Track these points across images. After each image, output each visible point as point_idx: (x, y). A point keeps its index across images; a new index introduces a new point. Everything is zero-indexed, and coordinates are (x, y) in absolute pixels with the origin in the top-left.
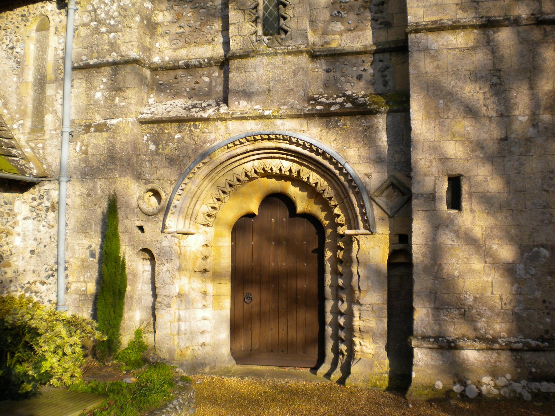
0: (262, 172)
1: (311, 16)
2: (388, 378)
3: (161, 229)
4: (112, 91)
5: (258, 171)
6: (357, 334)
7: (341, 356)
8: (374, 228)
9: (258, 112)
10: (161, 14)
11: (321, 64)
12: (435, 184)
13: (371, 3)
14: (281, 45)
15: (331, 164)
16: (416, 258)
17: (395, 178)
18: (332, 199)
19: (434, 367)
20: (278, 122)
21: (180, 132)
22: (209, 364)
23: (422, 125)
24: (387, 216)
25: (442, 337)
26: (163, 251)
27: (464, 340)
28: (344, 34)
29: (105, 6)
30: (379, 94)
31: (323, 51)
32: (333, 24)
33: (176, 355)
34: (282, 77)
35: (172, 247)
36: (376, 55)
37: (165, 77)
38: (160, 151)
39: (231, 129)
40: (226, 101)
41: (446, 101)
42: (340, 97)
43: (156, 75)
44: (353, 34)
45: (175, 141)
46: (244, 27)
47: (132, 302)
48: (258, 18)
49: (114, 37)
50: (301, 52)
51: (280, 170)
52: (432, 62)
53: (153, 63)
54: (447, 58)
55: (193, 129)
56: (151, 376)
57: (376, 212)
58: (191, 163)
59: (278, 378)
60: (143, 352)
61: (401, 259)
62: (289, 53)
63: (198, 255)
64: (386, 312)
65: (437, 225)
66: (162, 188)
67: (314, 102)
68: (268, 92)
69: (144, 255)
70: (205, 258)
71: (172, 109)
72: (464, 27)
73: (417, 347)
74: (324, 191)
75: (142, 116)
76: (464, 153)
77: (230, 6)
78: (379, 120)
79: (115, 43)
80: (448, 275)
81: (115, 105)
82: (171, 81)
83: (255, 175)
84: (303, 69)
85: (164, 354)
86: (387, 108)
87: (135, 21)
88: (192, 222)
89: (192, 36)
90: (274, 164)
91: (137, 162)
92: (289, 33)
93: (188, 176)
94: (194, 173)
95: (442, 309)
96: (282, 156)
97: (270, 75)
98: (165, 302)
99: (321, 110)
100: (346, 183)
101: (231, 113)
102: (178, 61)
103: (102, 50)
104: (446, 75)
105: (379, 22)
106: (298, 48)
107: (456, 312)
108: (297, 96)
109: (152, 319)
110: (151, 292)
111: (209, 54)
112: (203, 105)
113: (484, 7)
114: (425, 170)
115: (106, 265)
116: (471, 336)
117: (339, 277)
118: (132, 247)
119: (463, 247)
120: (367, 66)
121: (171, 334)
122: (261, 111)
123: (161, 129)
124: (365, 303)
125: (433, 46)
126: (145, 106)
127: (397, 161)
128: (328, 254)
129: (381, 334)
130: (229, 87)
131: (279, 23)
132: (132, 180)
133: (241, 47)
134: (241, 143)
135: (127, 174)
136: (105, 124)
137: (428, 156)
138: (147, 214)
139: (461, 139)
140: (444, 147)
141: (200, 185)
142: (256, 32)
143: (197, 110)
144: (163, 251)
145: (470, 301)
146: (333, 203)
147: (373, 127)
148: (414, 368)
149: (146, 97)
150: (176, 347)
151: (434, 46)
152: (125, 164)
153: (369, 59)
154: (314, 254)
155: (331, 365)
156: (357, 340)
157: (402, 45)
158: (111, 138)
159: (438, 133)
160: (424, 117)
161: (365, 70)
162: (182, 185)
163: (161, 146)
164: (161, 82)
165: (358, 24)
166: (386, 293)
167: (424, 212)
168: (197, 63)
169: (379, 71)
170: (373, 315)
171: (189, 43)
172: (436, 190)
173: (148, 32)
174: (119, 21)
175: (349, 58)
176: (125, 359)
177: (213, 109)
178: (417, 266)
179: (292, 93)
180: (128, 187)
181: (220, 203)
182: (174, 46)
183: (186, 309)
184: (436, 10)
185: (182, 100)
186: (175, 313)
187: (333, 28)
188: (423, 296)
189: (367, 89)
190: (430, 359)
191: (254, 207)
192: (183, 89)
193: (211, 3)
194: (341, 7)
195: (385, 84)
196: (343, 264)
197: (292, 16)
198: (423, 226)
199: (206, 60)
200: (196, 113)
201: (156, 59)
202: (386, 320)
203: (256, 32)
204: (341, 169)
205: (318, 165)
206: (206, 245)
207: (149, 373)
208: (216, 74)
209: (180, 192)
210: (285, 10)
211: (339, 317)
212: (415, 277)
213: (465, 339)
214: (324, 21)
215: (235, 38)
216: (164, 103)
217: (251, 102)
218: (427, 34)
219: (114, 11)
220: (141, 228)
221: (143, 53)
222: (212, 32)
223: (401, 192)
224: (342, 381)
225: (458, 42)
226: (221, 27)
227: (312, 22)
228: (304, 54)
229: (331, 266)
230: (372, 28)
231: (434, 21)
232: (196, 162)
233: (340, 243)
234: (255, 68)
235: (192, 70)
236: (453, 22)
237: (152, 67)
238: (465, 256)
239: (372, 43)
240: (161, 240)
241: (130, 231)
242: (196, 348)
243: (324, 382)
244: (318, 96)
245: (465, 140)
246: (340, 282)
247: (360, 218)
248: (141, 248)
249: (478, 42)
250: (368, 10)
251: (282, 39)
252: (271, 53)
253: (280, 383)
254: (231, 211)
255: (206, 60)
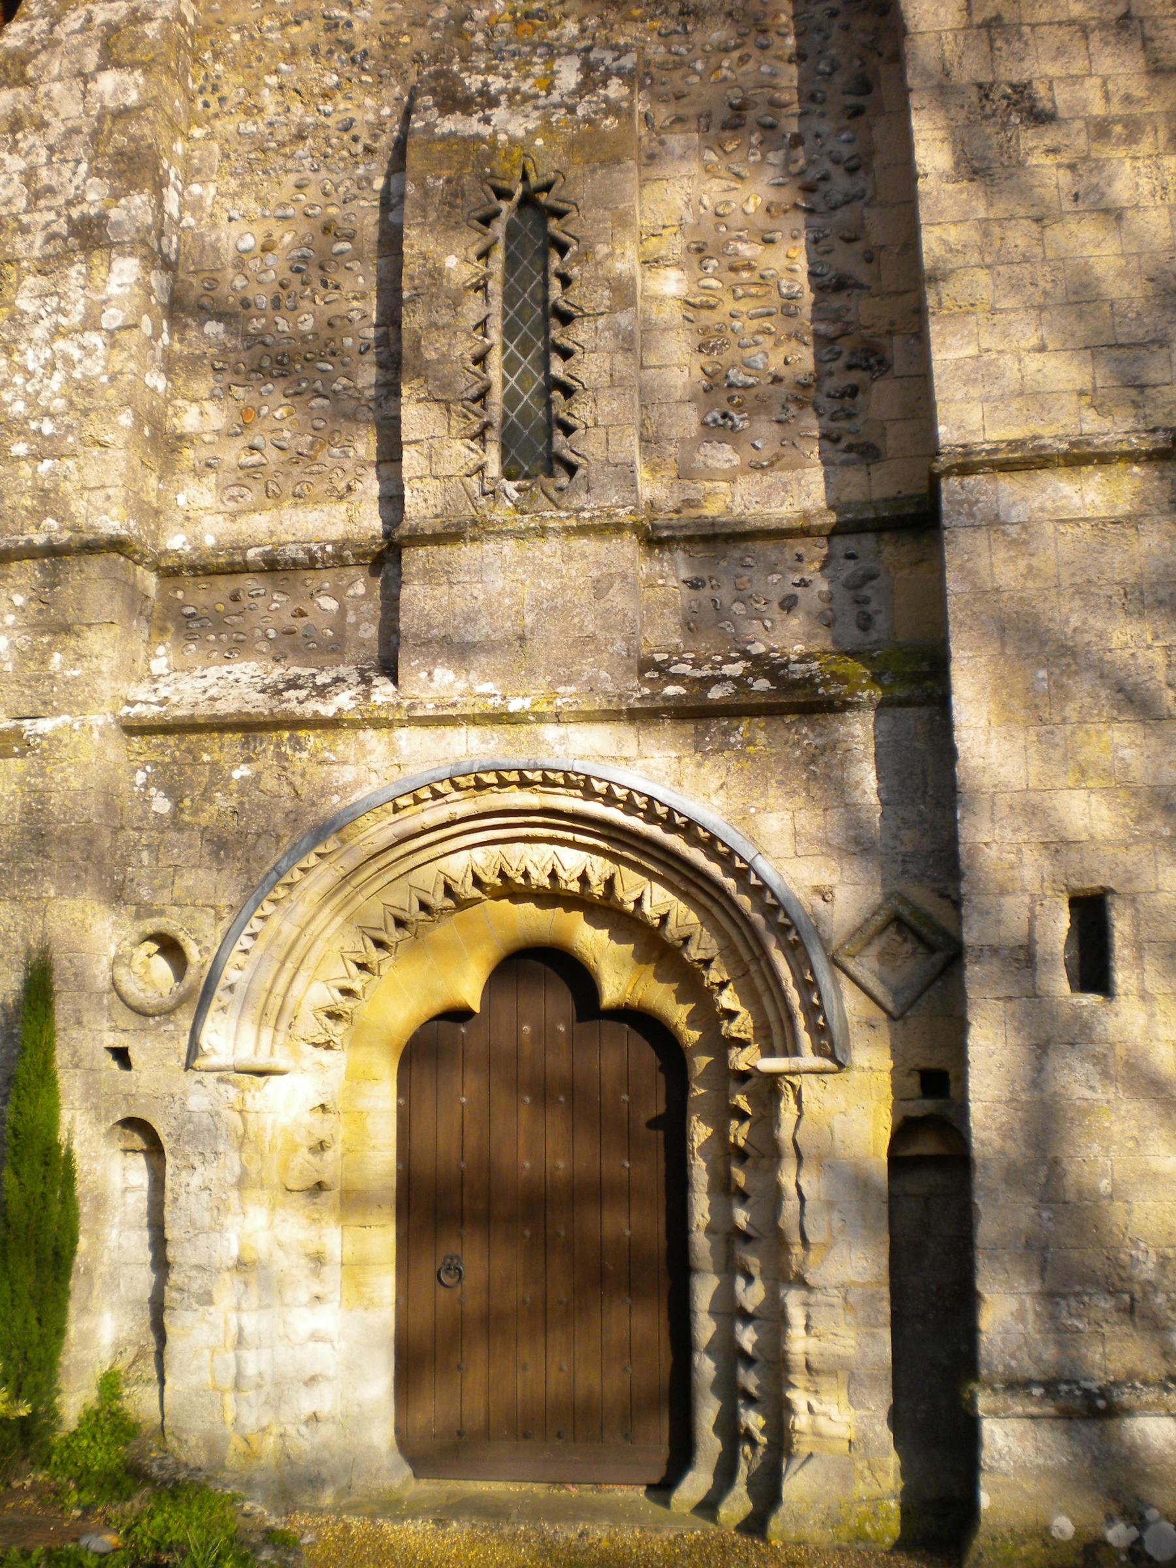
0: (498, 882)
1: (643, 425)
2: (898, 1513)
3: (184, 1058)
4: (43, 634)
5: (485, 879)
6: (798, 1378)
7: (747, 1448)
8: (847, 1051)
9: (491, 701)
10: (194, 409)
11: (674, 564)
12: (1032, 918)
13: (818, 389)
14: (558, 508)
15: (710, 858)
16: (982, 1143)
17: (904, 900)
18: (713, 965)
19: (1044, 1472)
20: (550, 732)
21: (248, 760)
22: (334, 1479)
23: (988, 742)
24: (884, 1015)
25: (1067, 1382)
26: (190, 1127)
27: (1134, 1387)
28: (740, 479)
29: (27, 380)
30: (847, 653)
31: (682, 527)
32: (707, 449)
33: (230, 1453)
34: (560, 601)
35: (218, 1114)
36: (836, 540)
37: (201, 595)
38: (186, 817)
39: (405, 752)
40: (390, 669)
41: (1057, 671)
42: (734, 661)
43: (176, 589)
44: (768, 479)
45: (233, 787)
46: (446, 452)
47: (91, 1286)
48: (487, 426)
49: (53, 473)
50: (619, 528)
51: (553, 876)
52: (1013, 559)
53: (165, 553)
54: (1057, 549)
55: (289, 752)
56: (168, 1529)
57: (849, 1005)
58: (279, 855)
59: (553, 1520)
60: (126, 1444)
61: (927, 1146)
62: (583, 530)
63: (298, 1140)
64: (888, 1310)
65: (1047, 1039)
66: (191, 931)
67: (656, 675)
68: (517, 643)
69: (127, 1138)
70: (321, 1147)
71: (224, 692)
72: (1103, 459)
73: (994, 1413)
74: (686, 940)
75: (134, 711)
76: (1115, 824)
77: (405, 391)
78: (852, 729)
79: (56, 489)
80: (1080, 1192)
81: (51, 677)
82: (220, 607)
83: (476, 893)
84: (625, 577)
85: (192, 1452)
86: (878, 694)
87: (116, 428)
88: (280, 1037)
89: (288, 475)
90: (536, 859)
91: (114, 848)
92: (581, 472)
93: (273, 896)
94: (290, 885)
95: (1064, 1296)
96: (560, 834)
97: (526, 593)
98: (195, 1287)
99: (679, 697)
100: (757, 917)
101: (406, 703)
102: (244, 550)
103: (14, 508)
104: (1054, 598)
105: (842, 445)
106: (609, 515)
107: (1106, 1303)
108: (605, 656)
109: (152, 1339)
110: (148, 1256)
111: (337, 531)
112: (321, 679)
113: (1160, 401)
114: (1000, 877)
115: (17, 1173)
116: (1153, 1374)
117: (735, 1201)
118: (92, 1114)
119: (1123, 1108)
120: (811, 570)
121: (215, 1388)
122: (498, 701)
123: (189, 751)
124: (822, 1283)
125: (1014, 513)
126: (141, 680)
127: (910, 849)
128: (700, 1132)
129: (873, 1378)
130: (402, 626)
131: (550, 443)
132: (96, 904)
133: (439, 511)
134: (437, 795)
135: (82, 886)
136: (17, 734)
137: (1008, 835)
138: (140, 1012)
139: (1105, 783)
140: (1055, 808)
141: (308, 923)
142: (481, 469)
143: (303, 693)
144: (190, 1127)
145: (1147, 1269)
146: (714, 975)
147: (834, 748)
148: (984, 1480)
149: (143, 654)
150: (229, 1429)
151: (1018, 513)
152: (76, 855)
153: (817, 550)
154: (654, 1133)
155: (715, 1475)
156: (798, 1398)
157: (912, 511)
158: (35, 776)
159: (1035, 766)
160: (993, 719)
161: (804, 584)
162: (254, 921)
163: (187, 802)
164: (189, 610)
165: (782, 451)
166: (885, 1249)
167: (1001, 1003)
168: (301, 555)
169: (847, 586)
170: (849, 1318)
171: (277, 496)
172: (1036, 936)
173: (154, 462)
174: (69, 426)
175: (758, 545)
176: (71, 1467)
177: (352, 693)
178: (985, 1167)
179: (591, 647)
180: (85, 928)
181: (366, 976)
182: (231, 505)
183: (260, 1307)
184: (1020, 410)
185: (253, 664)
186: (226, 1322)
187: (709, 462)
188: (1006, 1258)
189: (810, 637)
190: (1031, 1451)
191: (469, 989)
192: (258, 633)
193: (344, 381)
194: (730, 399)
195: (865, 623)
196: (749, 1162)
197: (590, 423)
198: (999, 1045)
199: (329, 548)
200: (296, 704)
201: (176, 541)
202: (886, 1335)
203: (481, 469)
204: (741, 876)
205: (671, 862)
206: (323, 1106)
207: (158, 1520)
208: (360, 589)
209: (245, 942)
210: (570, 405)
211: (739, 1327)
212: (979, 1201)
213: (1138, 1384)
214: (682, 440)
215: (417, 484)
216: (197, 673)
217: (468, 671)
218: (996, 479)
219: (55, 395)
220: (121, 1056)
221: (139, 522)
222: (348, 465)
223: (930, 939)
224: (755, 1525)
225: (1088, 500)
226: (373, 450)
227: (649, 442)
228: (628, 535)
229: (711, 1170)
230: (825, 463)
231: (1015, 441)
232: (296, 853)
233: (738, 1097)
234: (480, 571)
235: (285, 575)
236: (1071, 444)
237: (163, 564)
238: (1129, 1134)
239: (823, 504)
240: (184, 1093)
241: (86, 1064)
242: (291, 1430)
243: (698, 1530)
244: (666, 656)
245: (1118, 784)
246: (742, 1217)
247: (801, 1022)
248: (119, 1117)
249: (1145, 500)
250: (810, 409)
251: (560, 490)
252: (528, 529)
253: (561, 1538)
254: (402, 999)
255: (329, 548)
